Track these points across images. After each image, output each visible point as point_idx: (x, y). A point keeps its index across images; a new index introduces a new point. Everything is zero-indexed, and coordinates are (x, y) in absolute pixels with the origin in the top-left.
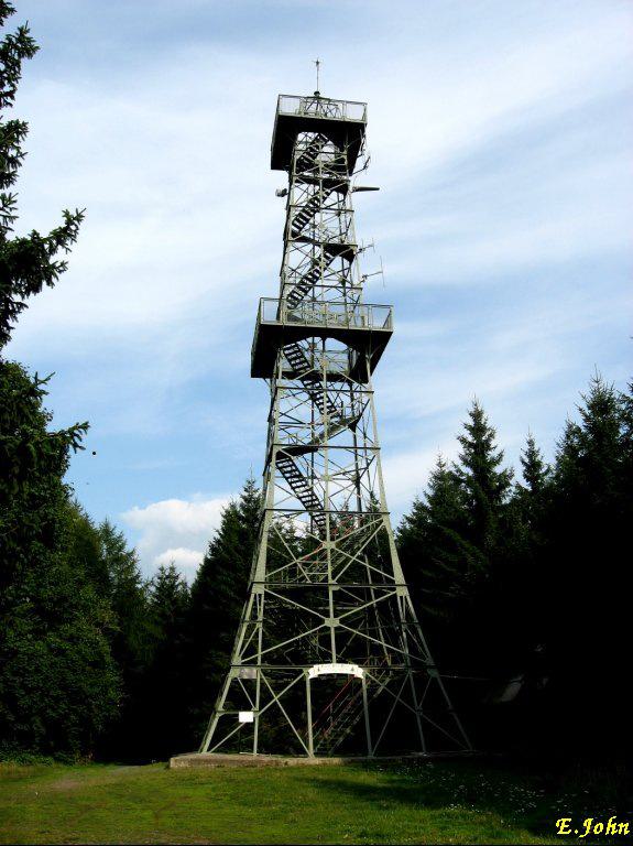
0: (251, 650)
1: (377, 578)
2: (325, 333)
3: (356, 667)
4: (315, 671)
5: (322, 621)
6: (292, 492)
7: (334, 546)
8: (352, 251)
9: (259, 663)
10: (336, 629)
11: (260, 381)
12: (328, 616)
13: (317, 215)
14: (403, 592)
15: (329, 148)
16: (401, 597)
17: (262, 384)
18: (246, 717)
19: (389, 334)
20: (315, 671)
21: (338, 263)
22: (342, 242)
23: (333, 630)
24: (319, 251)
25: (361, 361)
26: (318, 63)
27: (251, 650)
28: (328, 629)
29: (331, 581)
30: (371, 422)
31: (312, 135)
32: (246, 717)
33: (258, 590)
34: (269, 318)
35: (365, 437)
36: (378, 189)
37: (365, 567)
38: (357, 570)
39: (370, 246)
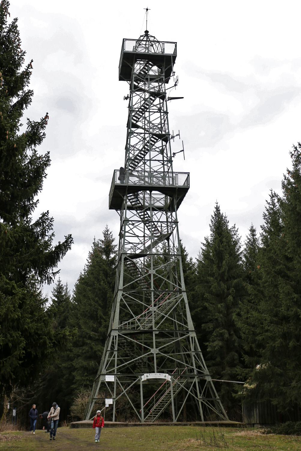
0: (112, 365)
2: (151, 189)
3: (167, 375)
4: (145, 377)
7: (154, 273)
8: (167, 138)
9: (116, 373)
10: (157, 354)
12: (152, 348)
14: (193, 335)
16: (192, 338)
18: (109, 402)
20: (145, 377)
21: (157, 101)
24: (147, 95)
25: (172, 202)
26: (147, 9)
27: (112, 365)
29: (154, 329)
33: (115, 333)
36: (183, 98)
39: (177, 135)
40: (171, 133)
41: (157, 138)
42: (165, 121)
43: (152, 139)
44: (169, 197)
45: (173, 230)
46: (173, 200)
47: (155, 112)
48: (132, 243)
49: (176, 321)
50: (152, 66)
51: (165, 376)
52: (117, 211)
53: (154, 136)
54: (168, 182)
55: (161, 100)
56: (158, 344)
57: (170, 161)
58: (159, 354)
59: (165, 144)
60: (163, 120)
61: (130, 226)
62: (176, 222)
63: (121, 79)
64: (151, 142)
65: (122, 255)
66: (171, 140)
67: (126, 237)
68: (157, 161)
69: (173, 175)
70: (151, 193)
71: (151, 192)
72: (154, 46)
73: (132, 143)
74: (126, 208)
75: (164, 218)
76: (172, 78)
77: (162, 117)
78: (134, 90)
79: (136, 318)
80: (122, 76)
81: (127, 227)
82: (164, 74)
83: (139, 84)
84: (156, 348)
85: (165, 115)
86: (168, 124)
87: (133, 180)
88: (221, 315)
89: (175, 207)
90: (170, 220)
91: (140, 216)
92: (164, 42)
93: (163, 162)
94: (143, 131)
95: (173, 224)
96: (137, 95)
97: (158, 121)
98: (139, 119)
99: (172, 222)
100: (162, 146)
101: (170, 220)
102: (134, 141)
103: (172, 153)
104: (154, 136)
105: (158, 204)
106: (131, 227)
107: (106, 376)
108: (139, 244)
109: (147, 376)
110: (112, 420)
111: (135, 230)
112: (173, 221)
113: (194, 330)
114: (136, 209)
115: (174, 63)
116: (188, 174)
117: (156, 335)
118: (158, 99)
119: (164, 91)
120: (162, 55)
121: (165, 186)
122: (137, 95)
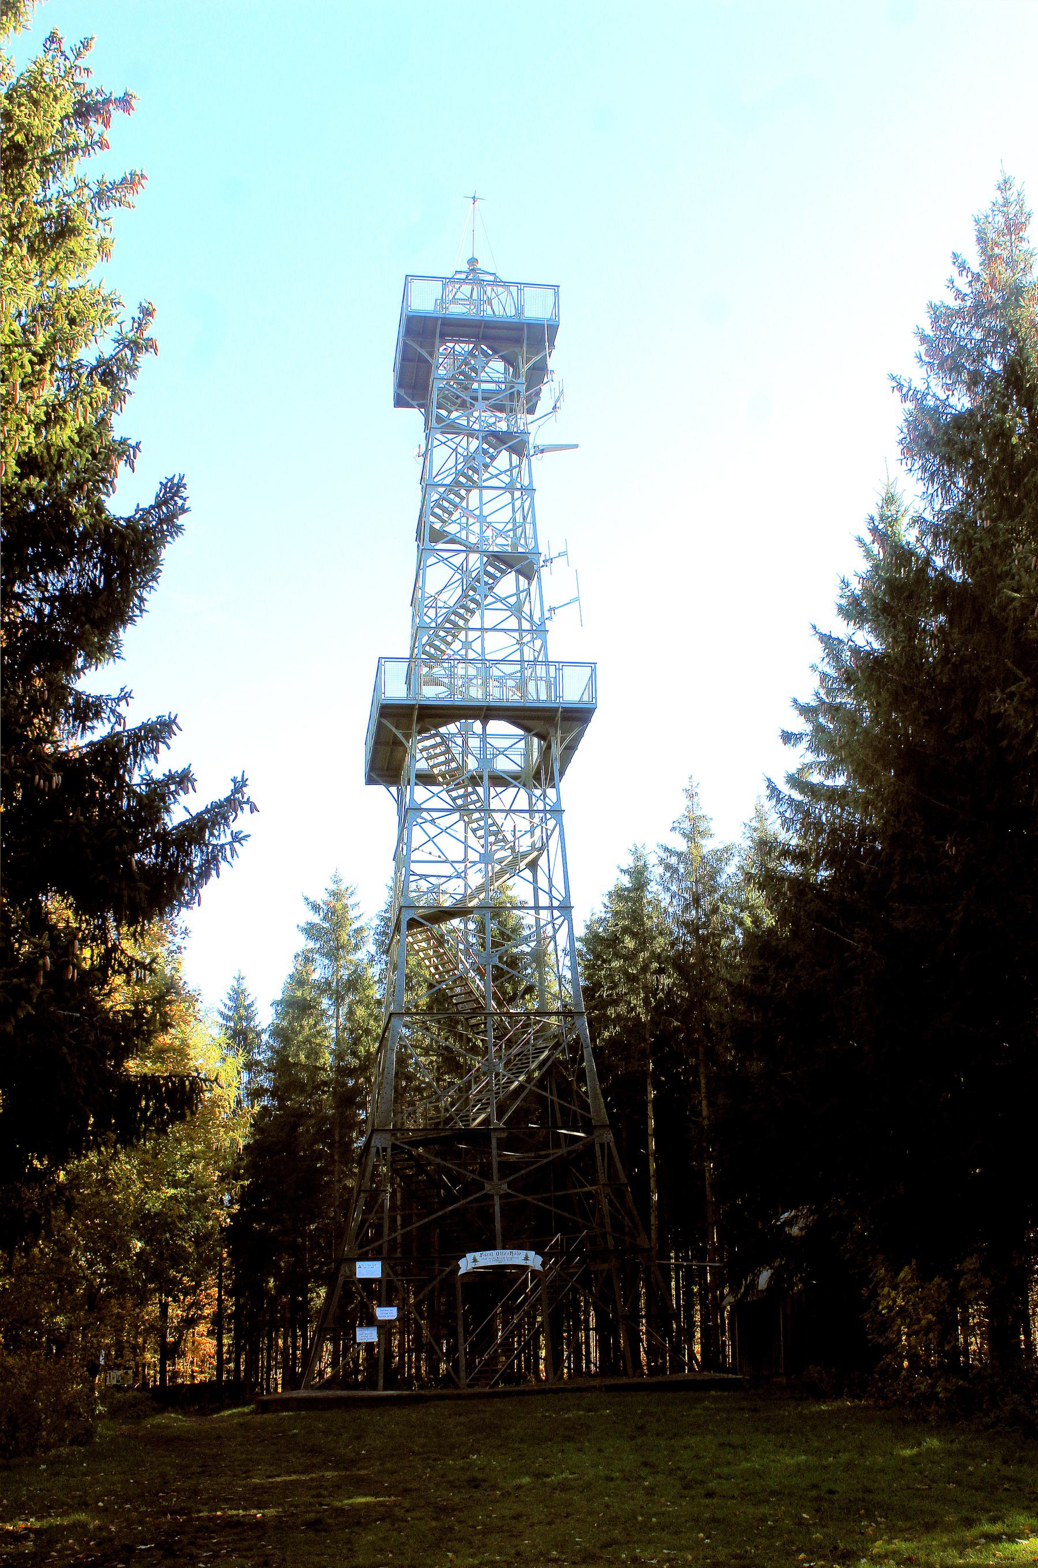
2: (486, 713)
8: (532, 564)
11: (380, 789)
12: (491, 1179)
13: (475, 494)
15: (497, 367)
16: (602, 1145)
17: (382, 796)
21: (508, 584)
22: (515, 546)
23: (497, 1199)
25: (546, 753)
28: (489, 1197)
31: (462, 348)
34: (396, 691)
36: (576, 446)
40: (542, 549)
42: (525, 518)
43: (490, 569)
44: (536, 740)
45: (548, 838)
46: (549, 747)
49: (555, 1099)
51: (526, 1258)
54: (538, 694)
55: (521, 578)
57: (539, 631)
58: (508, 1196)
59: (526, 587)
60: (520, 510)
61: (427, 826)
62: (557, 812)
63: (400, 402)
64: (486, 579)
65: (403, 910)
66: (544, 571)
67: (412, 865)
68: (502, 633)
69: (548, 672)
73: (431, 588)
74: (413, 780)
76: (545, 389)
77: (518, 504)
78: (436, 426)
80: (402, 393)
81: (416, 830)
82: (522, 380)
85: (559, 922)
86: (534, 524)
89: (557, 766)
90: (540, 806)
92: (521, 285)
93: (521, 636)
95: (548, 816)
96: (465, 843)
97: (506, 514)
98: (451, 514)
99: (544, 811)
101: (544, 900)
103: (546, 608)
105: (503, 765)
106: (432, 830)
107: (358, 1264)
108: (450, 877)
109: (475, 1260)
111: (443, 840)
112: (548, 808)
115: (552, 345)
116: (593, 666)
118: (504, 455)
119: (522, 428)
120: (516, 320)
121: (528, 705)
122: (465, 843)
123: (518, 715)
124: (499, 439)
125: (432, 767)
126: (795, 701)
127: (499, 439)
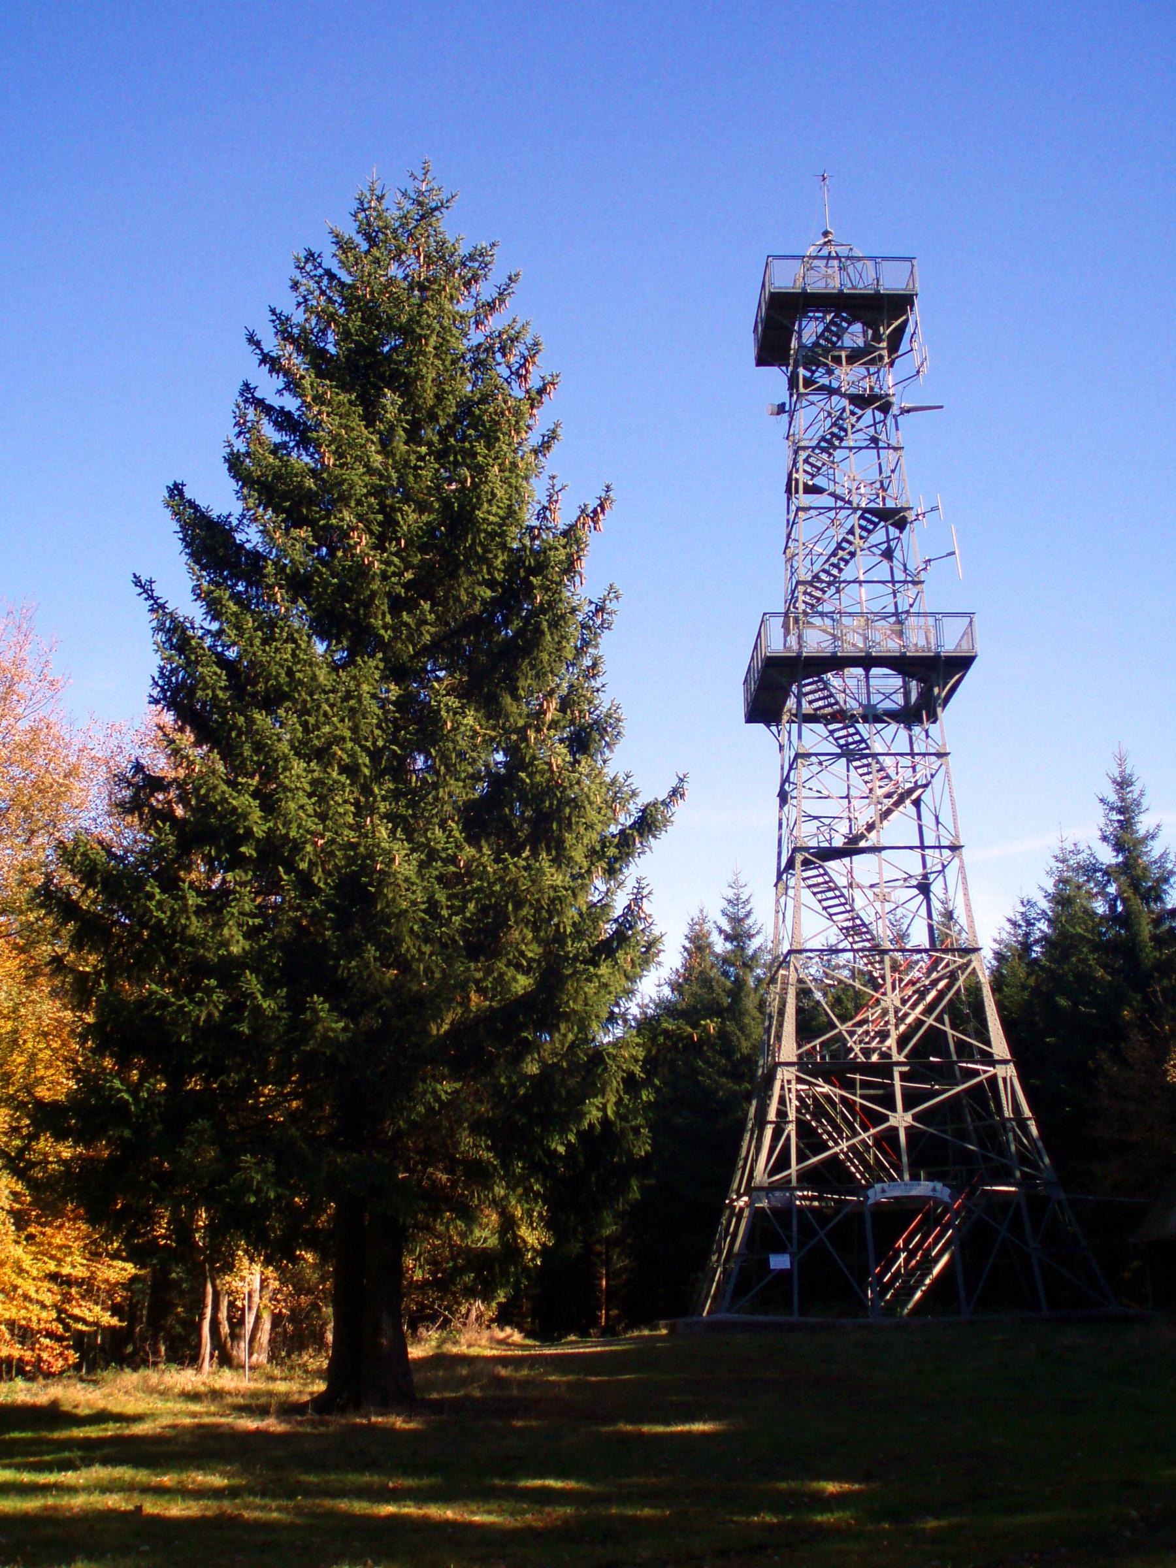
1: (964, 1050)
5: (885, 1118)
6: (824, 913)
10: (906, 1128)
12: (894, 1110)
16: (1004, 1079)
18: (780, 1262)
19: (962, 663)
29: (896, 1057)
30: (947, 794)
32: (780, 1262)
34: (776, 644)
35: (938, 823)
36: (941, 407)
37: (945, 1032)
38: (934, 1039)
41: (876, 520)
47: (860, 448)
48: (816, 818)
50: (850, 324)
51: (934, 1190)
52: (768, 726)
53: (867, 515)
56: (911, 1101)
58: (912, 1127)
63: (761, 361)
68: (880, 585)
70: (867, 677)
71: (867, 670)
72: (850, 269)
75: (902, 745)
79: (843, 1028)
82: (884, 344)
83: (813, 372)
84: (906, 1109)
87: (816, 641)
88: (431, 403)
91: (836, 739)
94: (830, 501)
100: (888, 541)
102: (807, 529)
104: (867, 515)
110: (791, 1315)
113: (1009, 1057)
114: (826, 720)
117: (901, 1073)
123: (902, 664)
124: (861, 401)
125: (816, 709)
126: (176, 490)
127: (861, 401)
